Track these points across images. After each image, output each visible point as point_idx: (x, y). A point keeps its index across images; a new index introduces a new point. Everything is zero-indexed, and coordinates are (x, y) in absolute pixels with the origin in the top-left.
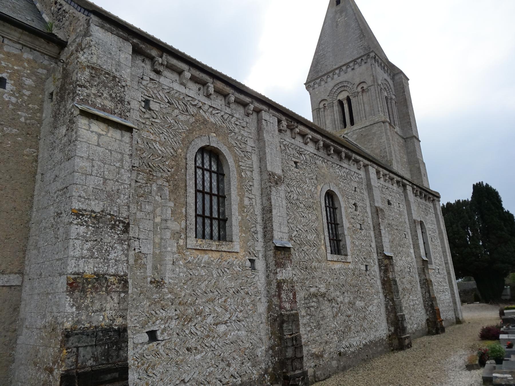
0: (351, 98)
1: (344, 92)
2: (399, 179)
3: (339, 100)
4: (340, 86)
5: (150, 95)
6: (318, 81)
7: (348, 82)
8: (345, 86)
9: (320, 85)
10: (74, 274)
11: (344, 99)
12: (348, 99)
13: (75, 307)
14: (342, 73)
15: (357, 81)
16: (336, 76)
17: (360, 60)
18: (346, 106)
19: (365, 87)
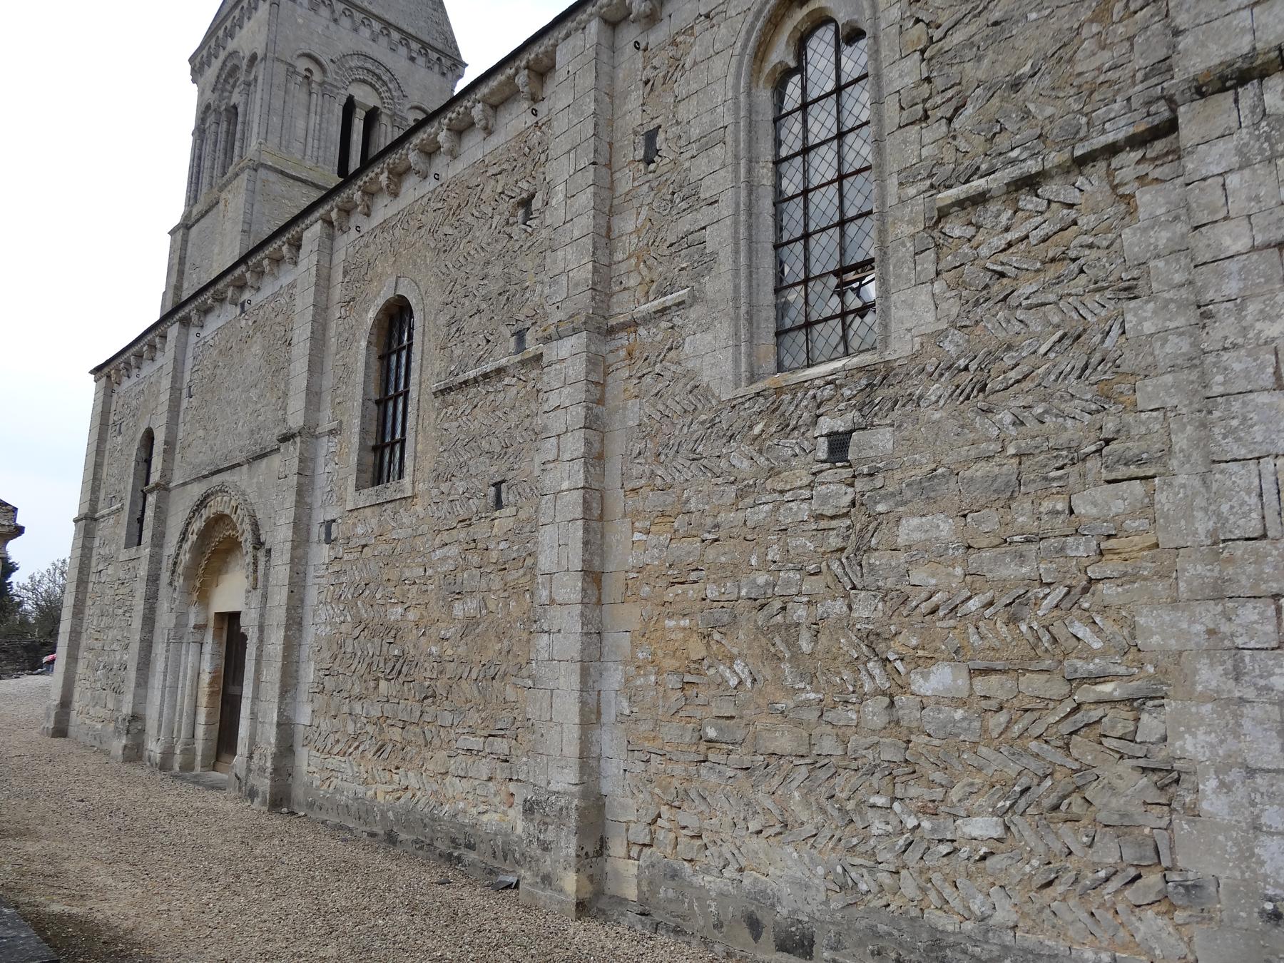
0: (384, 119)
1: (368, 88)
4: (368, 65)
7: (393, 78)
8: (379, 78)
11: (363, 106)
16: (365, 32)
17: (436, 56)
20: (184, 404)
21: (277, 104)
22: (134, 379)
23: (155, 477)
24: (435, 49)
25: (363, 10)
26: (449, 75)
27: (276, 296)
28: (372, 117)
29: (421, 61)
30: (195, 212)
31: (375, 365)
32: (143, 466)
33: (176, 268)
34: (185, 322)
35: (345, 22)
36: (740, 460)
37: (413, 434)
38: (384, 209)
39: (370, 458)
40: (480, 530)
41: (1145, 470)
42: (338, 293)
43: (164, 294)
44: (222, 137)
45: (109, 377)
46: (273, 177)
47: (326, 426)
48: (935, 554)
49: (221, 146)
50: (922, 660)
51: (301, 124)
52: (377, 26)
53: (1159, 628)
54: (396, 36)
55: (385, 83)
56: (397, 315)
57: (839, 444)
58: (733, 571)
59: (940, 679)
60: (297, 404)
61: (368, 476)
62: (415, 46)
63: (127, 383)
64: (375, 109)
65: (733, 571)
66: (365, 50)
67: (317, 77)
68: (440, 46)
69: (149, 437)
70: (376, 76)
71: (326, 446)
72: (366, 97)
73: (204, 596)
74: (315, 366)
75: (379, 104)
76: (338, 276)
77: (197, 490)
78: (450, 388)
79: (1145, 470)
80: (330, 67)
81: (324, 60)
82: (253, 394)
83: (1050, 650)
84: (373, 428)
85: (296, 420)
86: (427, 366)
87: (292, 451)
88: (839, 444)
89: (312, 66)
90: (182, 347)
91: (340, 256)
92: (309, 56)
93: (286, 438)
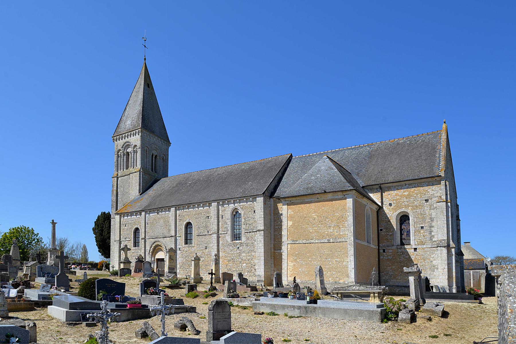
28: (156, 156)
36: (231, 248)
37: (143, 243)
40: (204, 251)
41: (255, 252)
48: (244, 256)
50: (243, 263)
53: (255, 261)
56: (189, 224)
57: (238, 248)
58: (230, 257)
59: (244, 265)
65: (230, 257)
72: (155, 153)
73: (154, 257)
77: (153, 240)
78: (501, 324)
79: (255, 252)
82: (162, 228)
83: (250, 263)
86: (195, 231)
88: (238, 248)
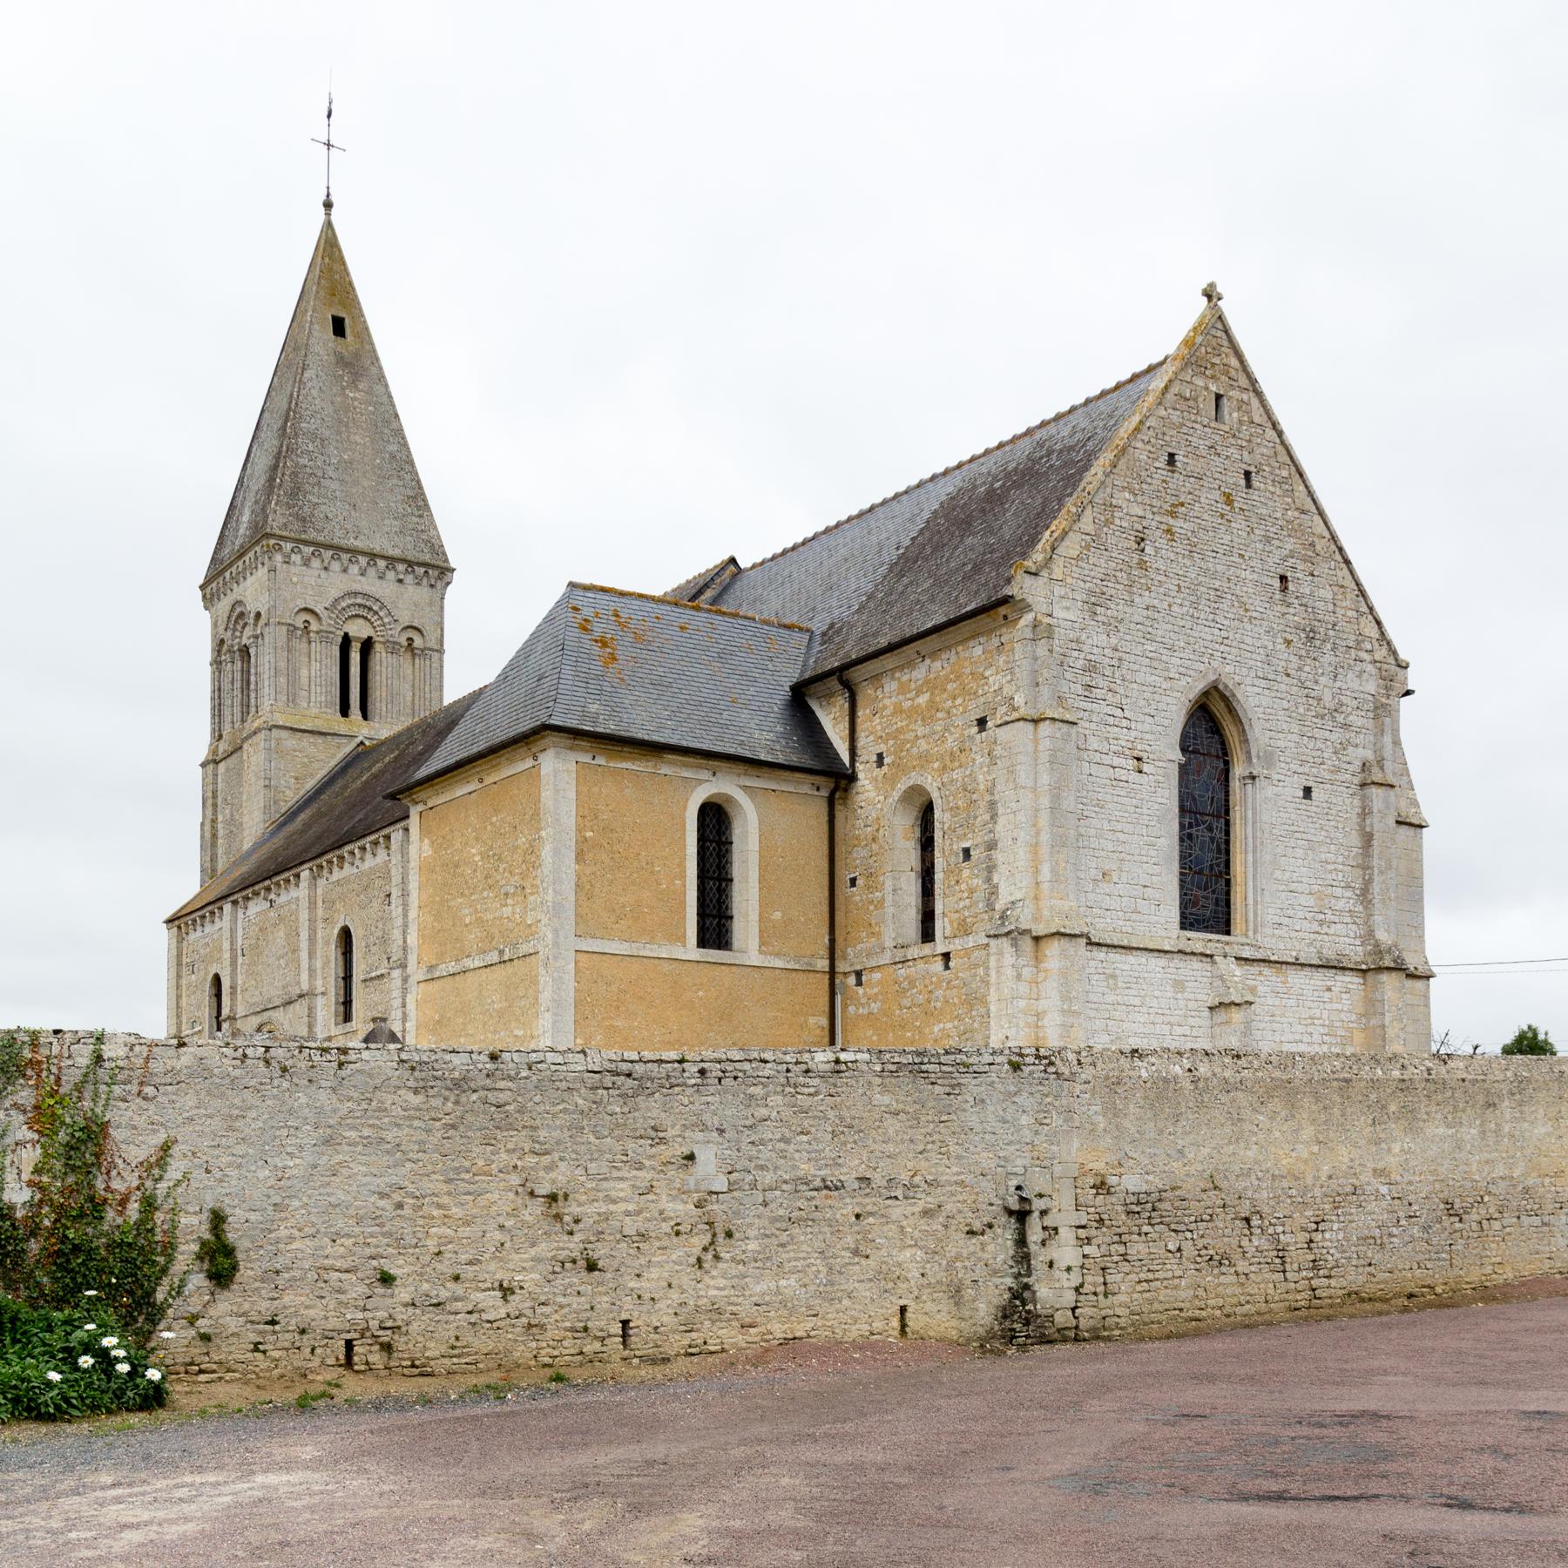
0: (378, 647)
1: (361, 621)
2: (320, 925)
3: (346, 635)
4: (359, 601)
5: (1507, 1505)
6: (308, 550)
7: (383, 606)
8: (370, 609)
9: (306, 563)
10: (1371, 1372)
11: (357, 639)
12: (367, 646)
13: (720, 1184)
14: (372, 572)
15: (405, 618)
16: (354, 569)
17: (422, 570)
18: (355, 657)
19: (418, 642)
20: (240, 960)
21: (282, 664)
22: (199, 933)
23: (225, 1012)
24: (420, 564)
25: (348, 551)
26: (439, 584)
27: (289, 902)
29: (409, 579)
30: (221, 750)
31: (340, 958)
32: (214, 999)
33: (210, 801)
34: (235, 903)
35: (336, 566)
38: (337, 874)
39: (342, 1008)
42: (320, 912)
43: (202, 824)
44: (238, 676)
45: (179, 927)
46: (284, 734)
47: (320, 989)
49: (238, 685)
51: (304, 672)
52: (363, 560)
54: (382, 563)
55: (376, 613)
60: (304, 976)
61: (341, 1018)
62: (401, 567)
63: (193, 936)
64: (370, 638)
66: (357, 587)
67: (314, 626)
68: (427, 558)
69: (217, 980)
70: (366, 607)
71: (320, 1001)
74: (311, 955)
75: (371, 632)
76: (320, 903)
80: (324, 614)
81: (319, 609)
84: (342, 992)
85: (305, 987)
87: (305, 1002)
89: (308, 617)
90: (234, 920)
91: (320, 891)
92: (306, 609)
93: (301, 996)
